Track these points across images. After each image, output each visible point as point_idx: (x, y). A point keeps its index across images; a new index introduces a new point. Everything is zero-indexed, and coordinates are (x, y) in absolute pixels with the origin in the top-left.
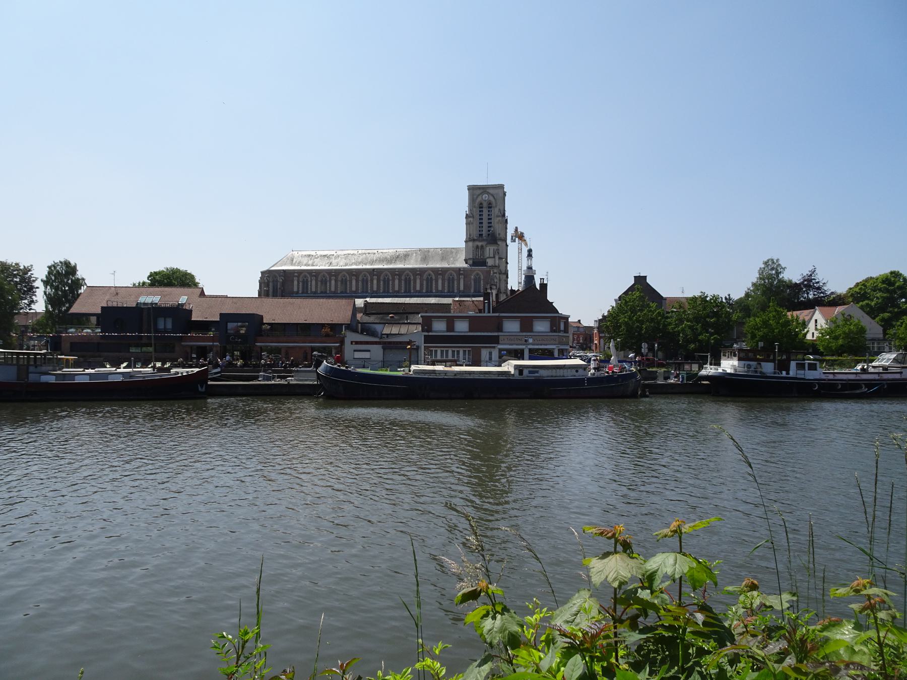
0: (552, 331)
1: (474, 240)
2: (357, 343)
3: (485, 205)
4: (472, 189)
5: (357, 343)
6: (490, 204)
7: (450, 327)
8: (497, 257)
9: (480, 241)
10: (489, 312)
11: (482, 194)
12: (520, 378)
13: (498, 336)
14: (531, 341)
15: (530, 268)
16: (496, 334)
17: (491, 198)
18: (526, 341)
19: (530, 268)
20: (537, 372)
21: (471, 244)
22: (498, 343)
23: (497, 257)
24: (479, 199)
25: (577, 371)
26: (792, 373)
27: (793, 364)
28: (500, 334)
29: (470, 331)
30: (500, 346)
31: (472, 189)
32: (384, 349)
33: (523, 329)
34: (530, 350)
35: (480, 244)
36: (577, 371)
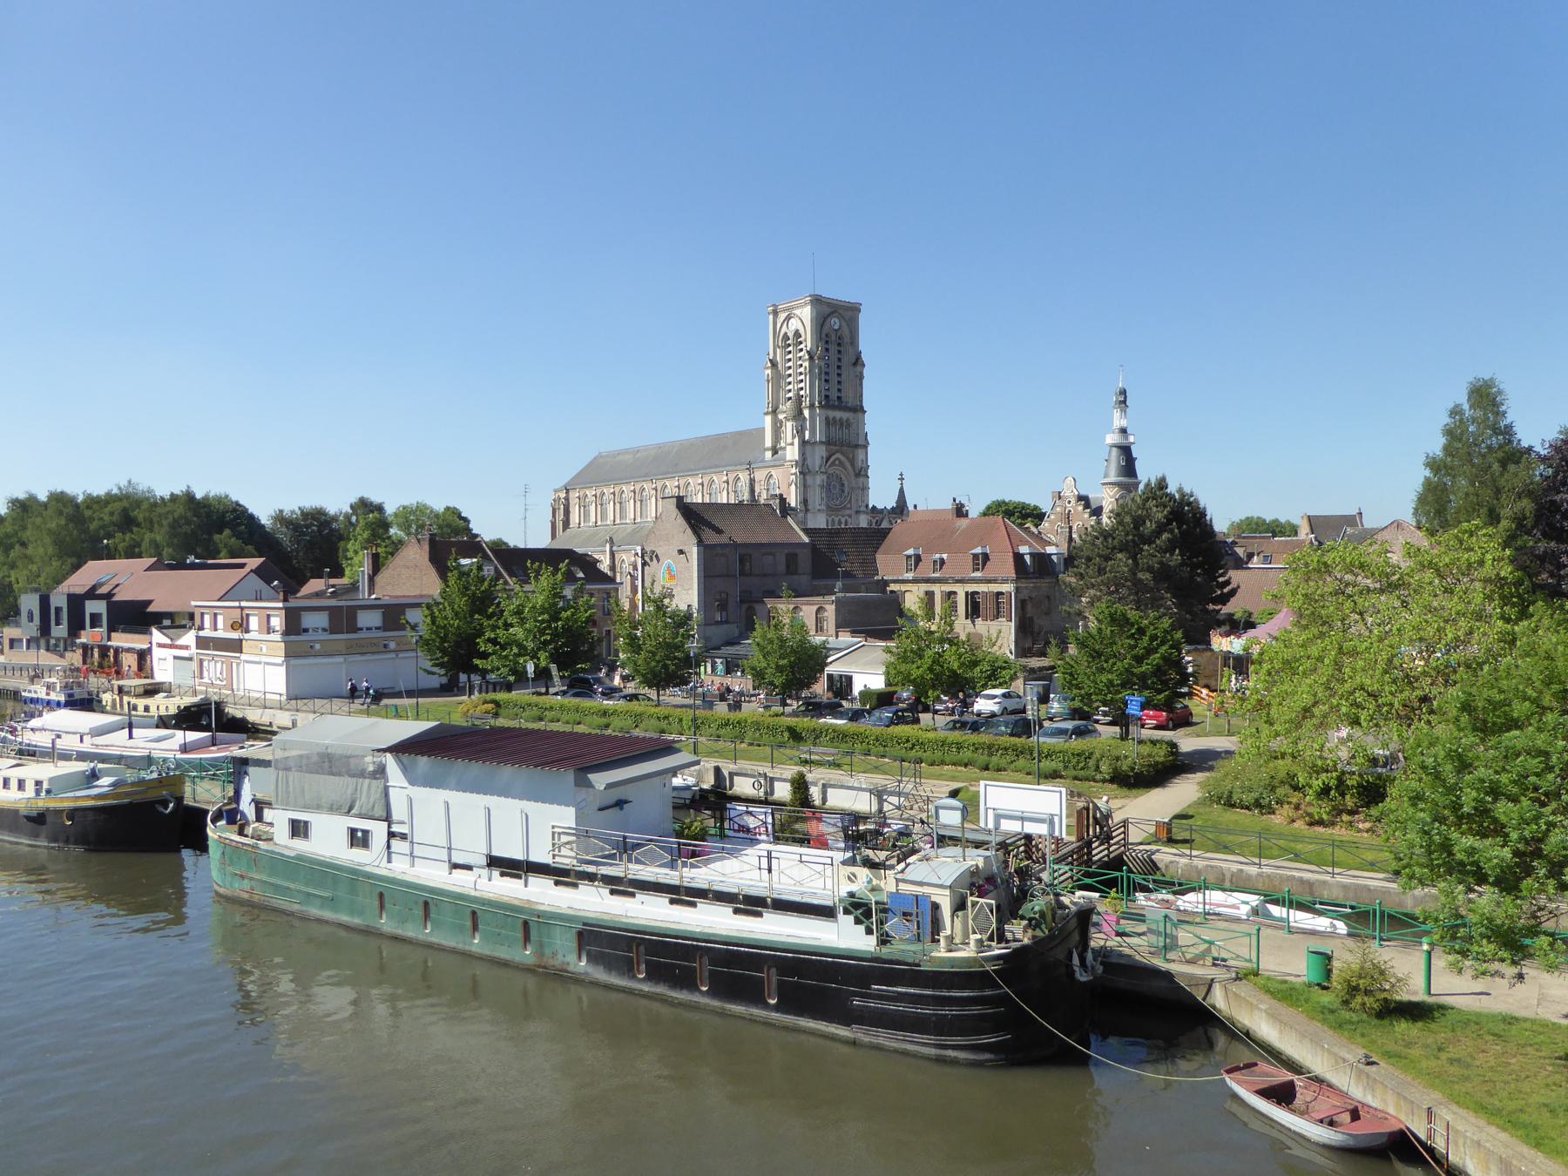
18: (385, 646)
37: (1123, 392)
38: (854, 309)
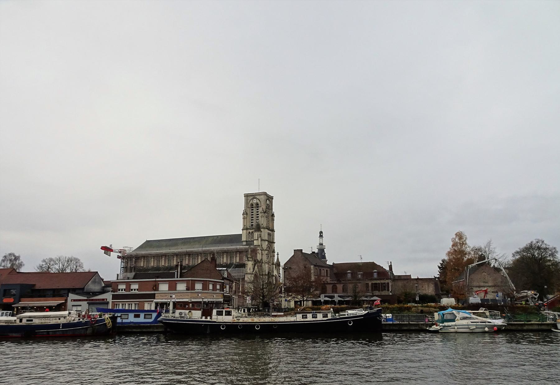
0: (187, 289)
1: (247, 229)
2: (75, 300)
3: (254, 206)
4: (247, 196)
5: (75, 300)
6: (258, 205)
7: (128, 288)
8: (259, 239)
9: (251, 229)
10: (177, 277)
11: (253, 199)
12: (21, 324)
13: (154, 294)
14: (174, 296)
15: (321, 244)
16: (153, 292)
17: (258, 201)
18: (171, 297)
19: (321, 244)
20: (32, 320)
21: (245, 231)
22: (154, 298)
23: (259, 239)
24: (251, 202)
25: (59, 319)
26: (330, 316)
27: (214, 312)
28: (155, 292)
29: (169, 290)
30: (155, 300)
31: (247, 196)
32: (89, 304)
33: (170, 288)
34: (174, 302)
35: (251, 231)
36: (59, 319)
37: (321, 232)
38: (272, 198)
